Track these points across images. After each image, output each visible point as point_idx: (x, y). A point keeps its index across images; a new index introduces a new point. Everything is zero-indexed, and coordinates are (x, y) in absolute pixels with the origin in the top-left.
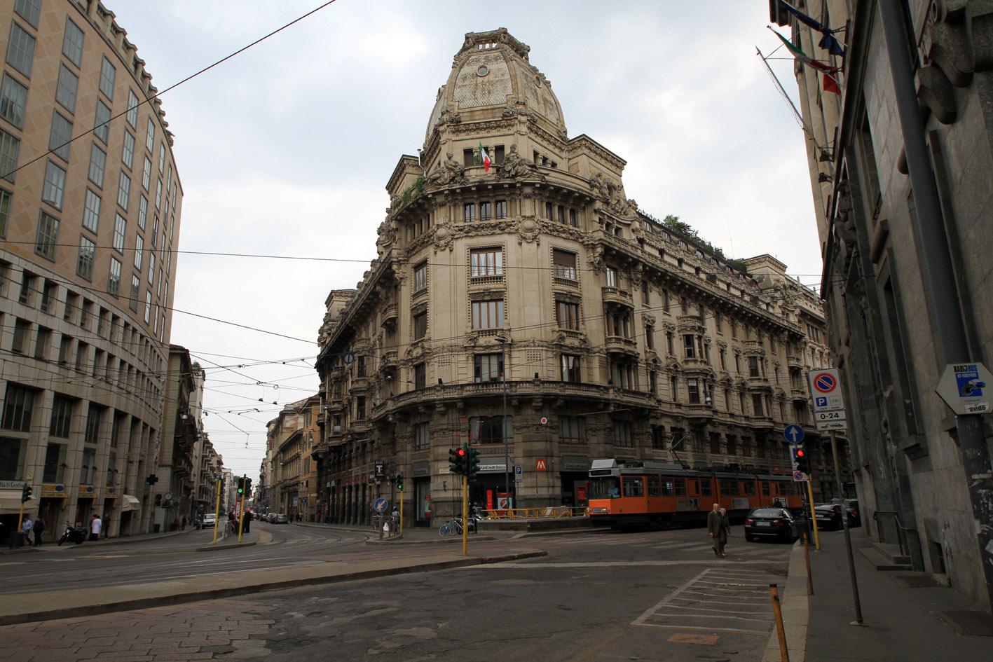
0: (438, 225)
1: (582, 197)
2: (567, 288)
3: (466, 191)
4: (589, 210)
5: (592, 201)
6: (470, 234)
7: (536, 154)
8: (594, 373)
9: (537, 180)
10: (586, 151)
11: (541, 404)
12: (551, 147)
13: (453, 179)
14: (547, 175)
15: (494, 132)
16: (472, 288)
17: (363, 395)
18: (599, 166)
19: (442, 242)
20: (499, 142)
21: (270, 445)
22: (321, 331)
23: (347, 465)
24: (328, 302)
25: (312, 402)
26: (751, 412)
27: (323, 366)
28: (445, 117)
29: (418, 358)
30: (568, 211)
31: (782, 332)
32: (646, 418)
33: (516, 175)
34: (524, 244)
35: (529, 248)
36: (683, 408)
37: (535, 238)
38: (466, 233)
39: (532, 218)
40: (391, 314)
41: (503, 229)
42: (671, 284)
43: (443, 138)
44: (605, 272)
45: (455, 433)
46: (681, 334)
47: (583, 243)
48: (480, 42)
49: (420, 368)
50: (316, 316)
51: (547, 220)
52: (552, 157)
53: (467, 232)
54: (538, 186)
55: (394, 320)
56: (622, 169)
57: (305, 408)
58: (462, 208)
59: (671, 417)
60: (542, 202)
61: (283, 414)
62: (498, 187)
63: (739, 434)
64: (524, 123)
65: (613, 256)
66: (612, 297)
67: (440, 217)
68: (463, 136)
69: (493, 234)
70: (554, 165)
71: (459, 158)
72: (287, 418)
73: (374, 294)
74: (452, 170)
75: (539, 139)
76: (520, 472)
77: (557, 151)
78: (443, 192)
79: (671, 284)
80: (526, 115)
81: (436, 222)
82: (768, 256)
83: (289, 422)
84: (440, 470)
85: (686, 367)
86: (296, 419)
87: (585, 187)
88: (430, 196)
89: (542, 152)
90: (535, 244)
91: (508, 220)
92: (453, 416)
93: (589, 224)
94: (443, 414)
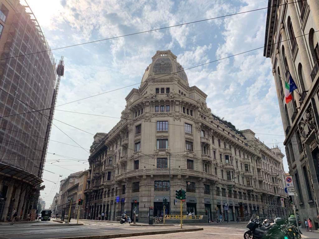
0: (146, 113)
1: (195, 106)
2: (189, 136)
3: (157, 101)
4: (197, 110)
5: (198, 108)
6: (157, 116)
7: (180, 91)
8: (198, 167)
9: (180, 100)
10: (196, 91)
11: (181, 177)
12: (184, 89)
13: (152, 97)
14: (184, 98)
15: (166, 83)
16: (157, 135)
17: (110, 171)
18: (199, 96)
19: (147, 118)
20: (168, 86)
21: (61, 189)
22: (91, 147)
23: (92, 199)
24: (95, 137)
25: (85, 173)
26: (245, 183)
27: (91, 160)
28: (150, 77)
29: (136, 158)
30: (190, 111)
31: (255, 156)
32: (214, 184)
33: (174, 98)
34: (176, 120)
35: (177, 122)
36: (225, 181)
37: (179, 119)
38: (156, 115)
39: (179, 112)
40: (126, 142)
41: (169, 115)
42: (221, 138)
43: (149, 84)
44: (201, 132)
45: (149, 186)
46: (224, 155)
47: (194, 121)
48: (162, 54)
49: (136, 163)
50: (90, 141)
51: (183, 113)
52: (184, 93)
53: (156, 115)
54: (181, 101)
55: (127, 144)
56: (206, 98)
57: (81, 175)
58: (154, 107)
59: (222, 184)
60: (182, 107)
61: (69, 177)
62: (168, 101)
63: (242, 191)
64: (176, 81)
65: (204, 126)
66: (204, 140)
67: (147, 110)
68: (156, 83)
69: (165, 117)
70: (185, 95)
71: (154, 92)
72: (71, 179)
73: (118, 135)
74: (152, 94)
75: (180, 86)
76: (176, 202)
77: (186, 91)
78: (149, 101)
79: (221, 138)
80: (177, 78)
81: (145, 111)
82: (250, 130)
83: (71, 180)
84: (143, 200)
85: (226, 167)
86: (74, 180)
87: (195, 103)
88: (144, 103)
89: (182, 91)
90: (179, 120)
91: (170, 112)
92: (149, 180)
93: (196, 115)
94: (145, 180)
